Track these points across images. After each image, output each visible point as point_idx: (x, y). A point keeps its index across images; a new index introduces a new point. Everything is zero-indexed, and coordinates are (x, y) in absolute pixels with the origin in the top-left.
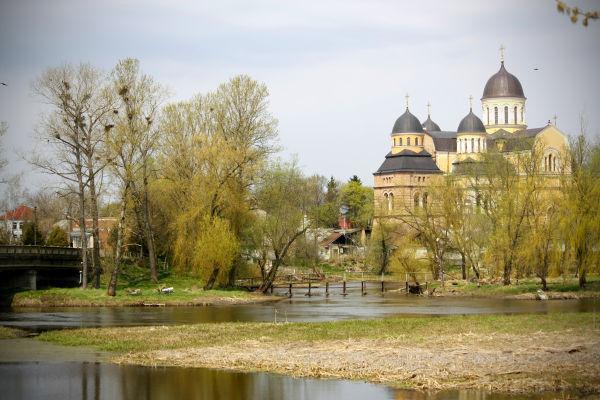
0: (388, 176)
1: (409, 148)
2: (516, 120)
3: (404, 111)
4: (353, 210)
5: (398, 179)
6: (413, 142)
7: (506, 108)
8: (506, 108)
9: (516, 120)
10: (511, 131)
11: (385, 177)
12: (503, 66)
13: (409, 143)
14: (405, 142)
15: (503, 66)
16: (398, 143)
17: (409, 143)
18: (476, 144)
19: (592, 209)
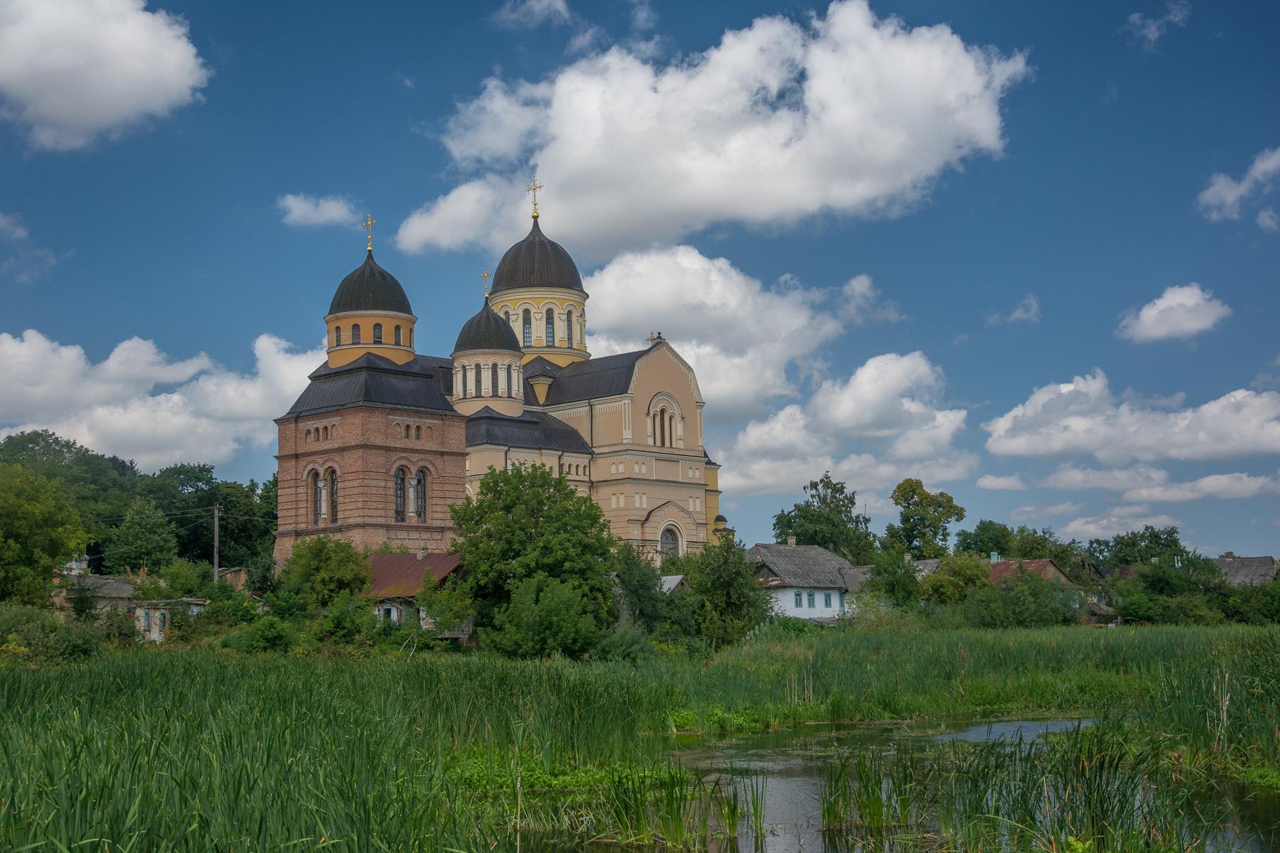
0: (320, 424)
1: (378, 350)
2: (570, 339)
3: (359, 263)
4: (187, 639)
5: (349, 428)
6: (388, 334)
7: (550, 313)
8: (550, 313)
9: (570, 339)
10: (563, 361)
11: (311, 425)
12: (536, 225)
13: (378, 341)
14: (367, 333)
15: (536, 225)
16: (347, 335)
17: (378, 341)
18: (486, 376)
19: (1004, 586)
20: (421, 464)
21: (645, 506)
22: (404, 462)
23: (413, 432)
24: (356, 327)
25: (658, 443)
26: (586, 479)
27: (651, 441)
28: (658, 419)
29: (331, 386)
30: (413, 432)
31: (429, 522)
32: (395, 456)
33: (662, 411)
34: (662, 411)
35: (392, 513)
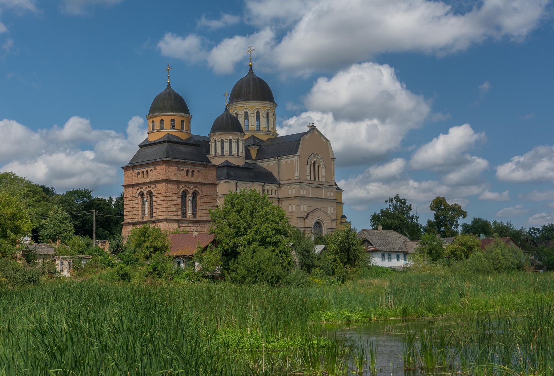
6: (178, 125)
20: (194, 189)
21: (306, 210)
22: (149, 189)
23: (190, 173)
24: (162, 121)
25: (312, 179)
26: (276, 197)
27: (308, 178)
28: (312, 167)
29: (149, 150)
30: (190, 173)
31: (198, 218)
32: (136, 189)
33: (314, 163)
34: (314, 163)
35: (180, 214)
